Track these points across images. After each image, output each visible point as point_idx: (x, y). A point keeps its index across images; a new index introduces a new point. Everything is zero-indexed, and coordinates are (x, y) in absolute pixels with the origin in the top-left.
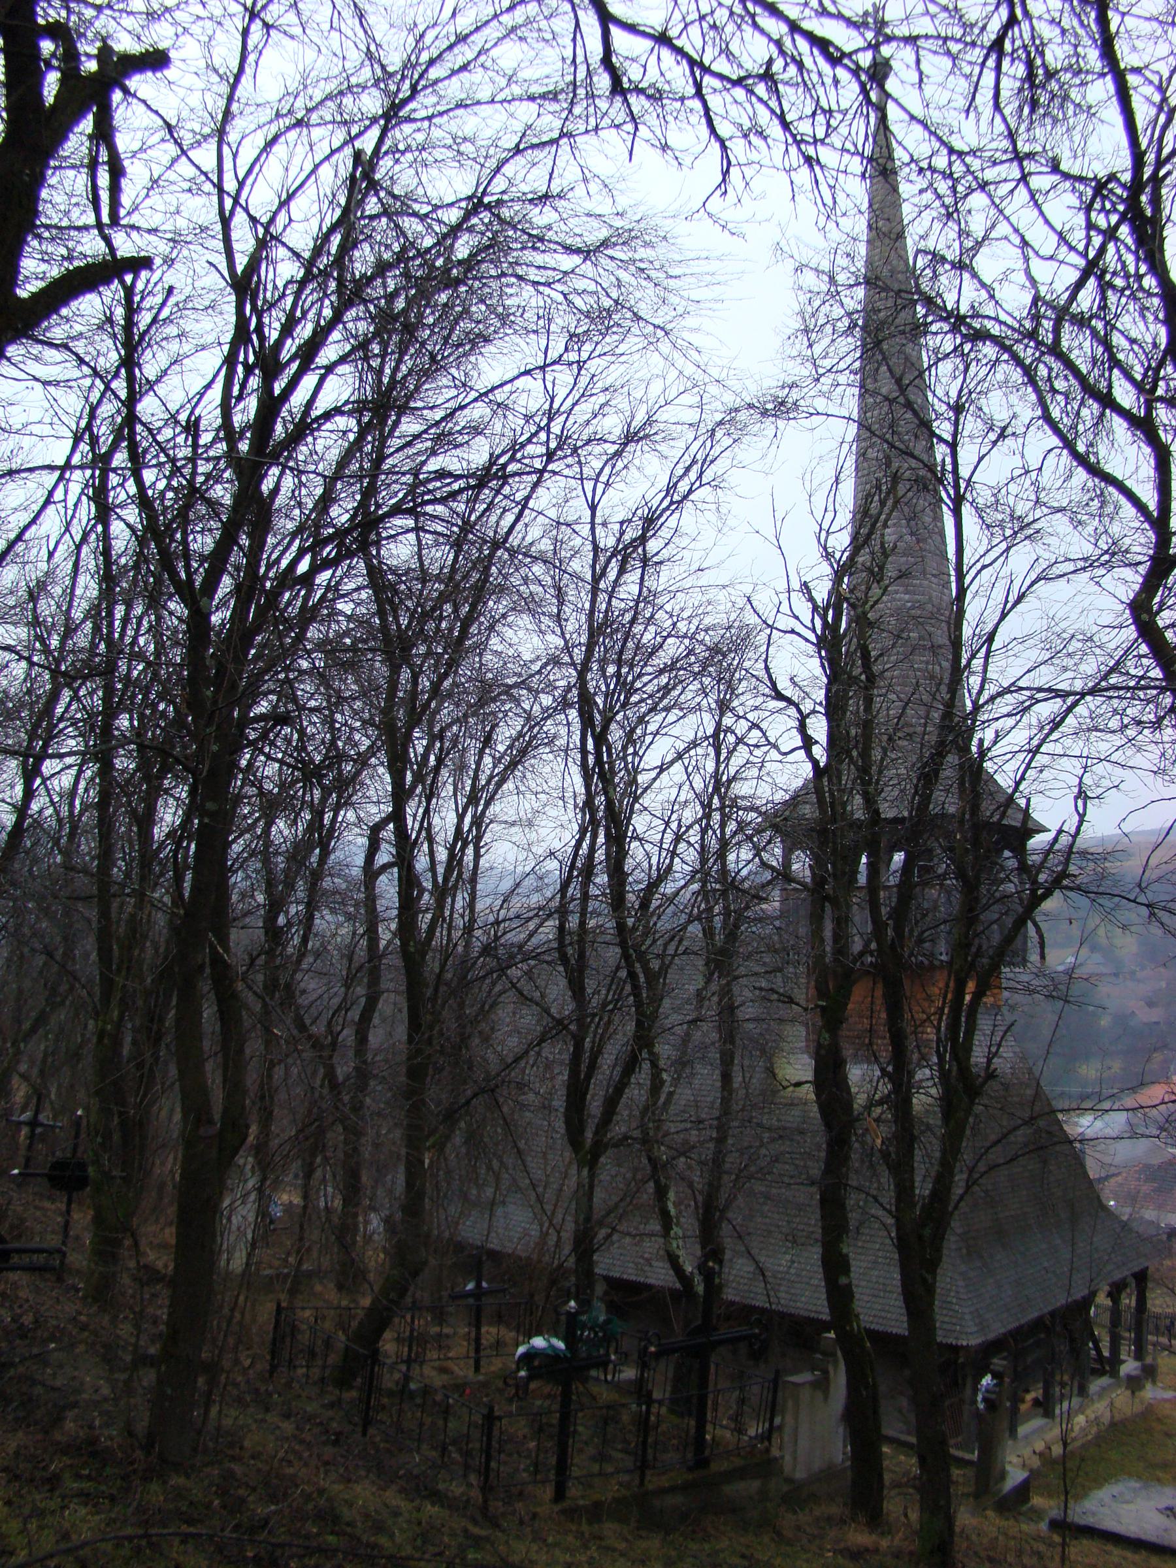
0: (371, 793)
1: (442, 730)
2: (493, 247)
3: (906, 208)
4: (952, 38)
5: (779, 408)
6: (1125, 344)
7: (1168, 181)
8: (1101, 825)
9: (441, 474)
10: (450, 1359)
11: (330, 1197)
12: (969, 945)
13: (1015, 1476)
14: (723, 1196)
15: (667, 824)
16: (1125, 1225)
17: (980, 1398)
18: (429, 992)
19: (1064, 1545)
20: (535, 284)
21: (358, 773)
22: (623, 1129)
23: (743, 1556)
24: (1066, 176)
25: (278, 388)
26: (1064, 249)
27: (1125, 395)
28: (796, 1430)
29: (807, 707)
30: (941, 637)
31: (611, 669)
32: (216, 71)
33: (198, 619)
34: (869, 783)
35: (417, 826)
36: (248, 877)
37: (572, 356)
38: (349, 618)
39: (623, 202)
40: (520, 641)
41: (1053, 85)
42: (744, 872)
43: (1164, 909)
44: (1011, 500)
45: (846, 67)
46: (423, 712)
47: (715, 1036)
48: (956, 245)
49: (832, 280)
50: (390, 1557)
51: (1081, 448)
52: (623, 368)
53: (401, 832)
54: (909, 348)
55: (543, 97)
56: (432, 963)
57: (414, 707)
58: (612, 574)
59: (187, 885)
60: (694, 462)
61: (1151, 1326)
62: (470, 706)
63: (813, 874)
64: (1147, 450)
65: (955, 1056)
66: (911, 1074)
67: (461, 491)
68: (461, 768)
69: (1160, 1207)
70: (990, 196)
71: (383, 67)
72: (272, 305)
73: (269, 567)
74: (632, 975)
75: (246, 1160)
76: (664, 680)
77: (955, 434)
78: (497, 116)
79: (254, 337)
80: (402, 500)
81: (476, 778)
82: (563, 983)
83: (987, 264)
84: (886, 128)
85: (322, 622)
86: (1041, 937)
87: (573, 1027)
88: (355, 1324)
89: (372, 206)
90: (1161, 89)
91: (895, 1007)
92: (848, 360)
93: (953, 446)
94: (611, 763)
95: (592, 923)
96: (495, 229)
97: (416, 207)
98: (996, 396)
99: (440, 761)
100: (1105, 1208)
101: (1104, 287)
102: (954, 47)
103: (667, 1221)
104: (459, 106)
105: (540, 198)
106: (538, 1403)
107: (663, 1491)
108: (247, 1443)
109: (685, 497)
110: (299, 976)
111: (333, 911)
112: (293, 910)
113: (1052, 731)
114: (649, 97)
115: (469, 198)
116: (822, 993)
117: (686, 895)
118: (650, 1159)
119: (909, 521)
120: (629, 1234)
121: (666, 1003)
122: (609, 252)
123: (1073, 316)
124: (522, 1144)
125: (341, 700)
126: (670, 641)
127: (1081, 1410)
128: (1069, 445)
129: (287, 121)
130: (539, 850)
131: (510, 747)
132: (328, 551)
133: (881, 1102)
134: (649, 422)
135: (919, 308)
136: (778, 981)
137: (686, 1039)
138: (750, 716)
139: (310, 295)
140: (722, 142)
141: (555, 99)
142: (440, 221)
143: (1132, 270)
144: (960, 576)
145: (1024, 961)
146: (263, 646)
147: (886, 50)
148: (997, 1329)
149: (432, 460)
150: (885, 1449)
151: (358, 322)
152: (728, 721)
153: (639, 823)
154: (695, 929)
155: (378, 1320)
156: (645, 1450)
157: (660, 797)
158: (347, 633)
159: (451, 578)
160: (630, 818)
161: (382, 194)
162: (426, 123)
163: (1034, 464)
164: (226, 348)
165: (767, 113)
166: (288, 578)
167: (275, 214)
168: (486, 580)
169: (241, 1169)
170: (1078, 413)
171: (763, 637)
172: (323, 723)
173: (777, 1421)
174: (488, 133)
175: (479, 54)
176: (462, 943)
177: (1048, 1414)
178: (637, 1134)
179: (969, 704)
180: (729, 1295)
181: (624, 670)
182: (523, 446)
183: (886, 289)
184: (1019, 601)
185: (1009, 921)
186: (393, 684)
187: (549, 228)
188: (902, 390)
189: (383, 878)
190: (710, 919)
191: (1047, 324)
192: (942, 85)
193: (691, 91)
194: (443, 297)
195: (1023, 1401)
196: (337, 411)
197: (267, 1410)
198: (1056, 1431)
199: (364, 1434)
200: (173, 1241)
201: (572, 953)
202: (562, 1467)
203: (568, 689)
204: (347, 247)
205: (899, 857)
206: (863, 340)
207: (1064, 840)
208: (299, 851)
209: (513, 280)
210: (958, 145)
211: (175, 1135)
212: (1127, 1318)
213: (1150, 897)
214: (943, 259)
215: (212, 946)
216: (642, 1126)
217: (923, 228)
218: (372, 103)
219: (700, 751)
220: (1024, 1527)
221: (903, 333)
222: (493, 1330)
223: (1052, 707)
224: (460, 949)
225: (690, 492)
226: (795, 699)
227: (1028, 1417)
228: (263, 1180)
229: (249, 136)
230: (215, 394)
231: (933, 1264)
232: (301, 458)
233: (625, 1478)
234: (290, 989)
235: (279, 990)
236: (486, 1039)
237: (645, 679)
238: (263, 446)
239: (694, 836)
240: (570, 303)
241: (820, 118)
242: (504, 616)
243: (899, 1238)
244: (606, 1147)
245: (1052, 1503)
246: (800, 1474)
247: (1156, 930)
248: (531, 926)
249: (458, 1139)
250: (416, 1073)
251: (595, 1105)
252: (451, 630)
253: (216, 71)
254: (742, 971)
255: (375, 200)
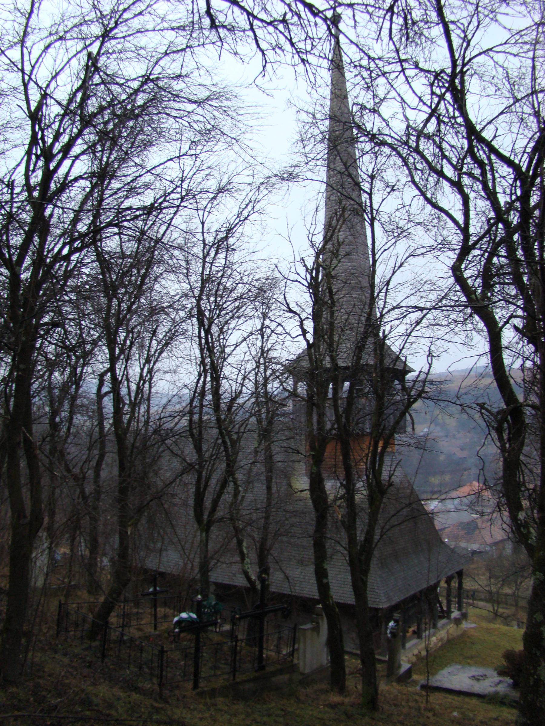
0: (99, 358)
1: (133, 328)
2: (154, 100)
3: (348, 84)
4: (370, 5)
5: (289, 177)
6: (448, 147)
7: (468, 73)
8: (439, 368)
9: (130, 208)
10: (142, 624)
11: (83, 550)
12: (380, 425)
13: (405, 666)
14: (269, 542)
15: (239, 371)
16: (453, 551)
17: (388, 631)
18: (128, 452)
19: (427, 695)
20: (175, 117)
21: (93, 349)
22: (222, 513)
23: (282, 710)
24: (422, 70)
25: (52, 166)
26: (421, 103)
27: (449, 171)
28: (305, 652)
29: (303, 316)
30: (366, 284)
31: (212, 299)
32: (19, 11)
33: (15, 278)
34: (333, 351)
35: (121, 374)
36: (41, 399)
37: (193, 152)
38: (88, 276)
39: (216, 80)
40: (170, 286)
41: (416, 28)
42: (275, 393)
43: (469, 407)
44: (397, 220)
45: (320, 17)
46: (123, 320)
47: (263, 469)
48: (372, 101)
49: (314, 117)
50: (117, 720)
51: (429, 195)
52: (216, 157)
53: (114, 377)
54: (349, 149)
55: (178, 28)
56: (130, 438)
57: (119, 318)
58: (212, 254)
59: (12, 403)
60: (250, 202)
61: (465, 595)
62: (146, 316)
63: (308, 394)
64: (459, 196)
65: (374, 476)
66: (354, 485)
67: (140, 215)
68: (142, 346)
69: (468, 541)
70: (387, 79)
71: (101, 12)
72: (50, 126)
73: (49, 252)
74: (224, 442)
75: (43, 534)
76: (237, 304)
77: (371, 189)
78: (156, 37)
79: (40, 142)
80: (112, 220)
81: (149, 351)
82: (192, 446)
83: (385, 110)
84: (339, 46)
85: (75, 278)
86: (413, 420)
87: (197, 467)
88: (97, 609)
89: (97, 79)
90: (464, 32)
91: (346, 455)
92: (322, 154)
93: (370, 194)
94: (213, 343)
95: (205, 418)
96: (155, 93)
97: (118, 80)
98: (390, 171)
99: (132, 343)
100: (443, 542)
101: (439, 122)
102: (371, 9)
103: (243, 556)
104: (139, 32)
105: (177, 77)
106: (185, 643)
107: (244, 682)
108: (46, 670)
109: (246, 218)
110: (66, 446)
111: (82, 415)
112: (63, 414)
113: (416, 326)
114: (228, 30)
115: (143, 76)
116: (312, 448)
117: (249, 404)
118: (234, 527)
119: (350, 229)
120: (225, 563)
121: (240, 455)
122: (210, 103)
123: (425, 135)
124: (174, 522)
125: (84, 315)
126: (240, 285)
127: (434, 635)
128: (423, 194)
129: (55, 37)
130: (180, 384)
131: (165, 336)
132: (77, 244)
133: (341, 498)
134: (229, 183)
135: (354, 130)
136: (292, 444)
137: (250, 471)
138: (277, 320)
139: (67, 122)
140: (262, 51)
141: (184, 30)
142: (129, 87)
143: (452, 114)
144: (374, 255)
145: (405, 432)
146: (46, 289)
147: (339, 10)
148: (396, 599)
149: (127, 200)
150: (346, 657)
151: (90, 136)
152: (267, 322)
153: (226, 371)
154: (253, 420)
155: (108, 608)
156: (235, 663)
157: (236, 359)
158: (87, 283)
159: (136, 256)
160: (221, 369)
161: (101, 74)
162: (122, 40)
163: (407, 203)
164: (27, 147)
165: (284, 38)
166: (58, 257)
167: (50, 82)
168: (152, 258)
169: (41, 538)
170: (427, 180)
171: (282, 284)
172: (76, 325)
173: (296, 646)
174: (152, 45)
175: (148, 7)
176: (144, 429)
177: (419, 637)
178: (228, 516)
179: (378, 314)
180: (273, 589)
181: (219, 299)
182: (169, 194)
183: (339, 121)
184: (400, 266)
185: (398, 414)
186: (109, 307)
187: (181, 91)
188: (347, 168)
189: (106, 399)
190: (260, 415)
191: (413, 138)
192: (365, 27)
193: (248, 27)
194: (131, 123)
195: (408, 632)
196: (81, 177)
197: (56, 652)
198: (423, 645)
199: (103, 662)
200: (8, 574)
201: (196, 432)
202: (197, 674)
203: (192, 308)
204: (86, 98)
205: (347, 384)
206: (328, 145)
207: (422, 376)
208: (65, 387)
209: (165, 116)
210: (372, 55)
211: (9, 522)
212: (454, 592)
213: (462, 402)
214: (365, 108)
215: (24, 434)
216: (231, 513)
217: (357, 94)
218: (96, 30)
219: (254, 336)
220: (410, 689)
221: (347, 142)
222: (163, 610)
223: (415, 316)
224: (143, 431)
225: (249, 216)
226: (298, 312)
227: (410, 639)
228: (51, 544)
229: (36, 43)
230: (22, 169)
231: (366, 572)
232: (64, 199)
233: (226, 676)
234: (62, 454)
235: (58, 452)
236: (156, 474)
237: (228, 303)
238: (44, 195)
239: (252, 377)
240: (191, 126)
241: (308, 41)
242: (161, 274)
243: (350, 560)
244: (214, 522)
245: (422, 677)
246: (307, 671)
247: (465, 416)
248: (176, 420)
249: (144, 521)
250: (123, 491)
251: (208, 503)
252: (136, 281)
253: (19, 11)
254: (275, 439)
255: (98, 76)
